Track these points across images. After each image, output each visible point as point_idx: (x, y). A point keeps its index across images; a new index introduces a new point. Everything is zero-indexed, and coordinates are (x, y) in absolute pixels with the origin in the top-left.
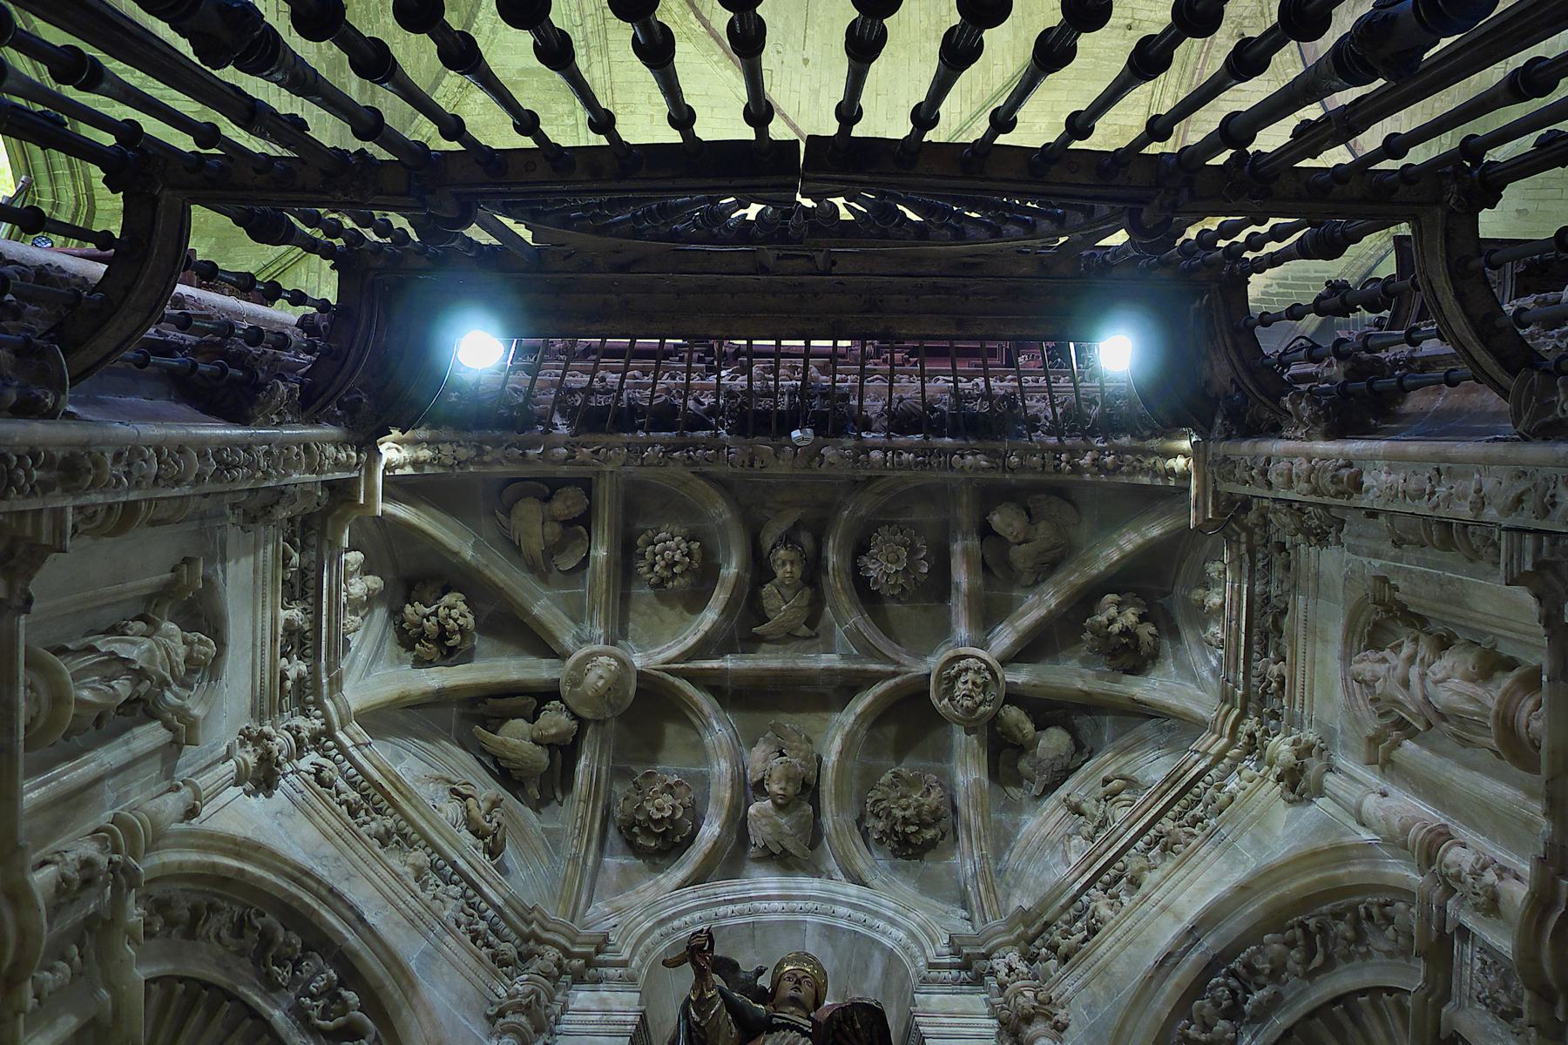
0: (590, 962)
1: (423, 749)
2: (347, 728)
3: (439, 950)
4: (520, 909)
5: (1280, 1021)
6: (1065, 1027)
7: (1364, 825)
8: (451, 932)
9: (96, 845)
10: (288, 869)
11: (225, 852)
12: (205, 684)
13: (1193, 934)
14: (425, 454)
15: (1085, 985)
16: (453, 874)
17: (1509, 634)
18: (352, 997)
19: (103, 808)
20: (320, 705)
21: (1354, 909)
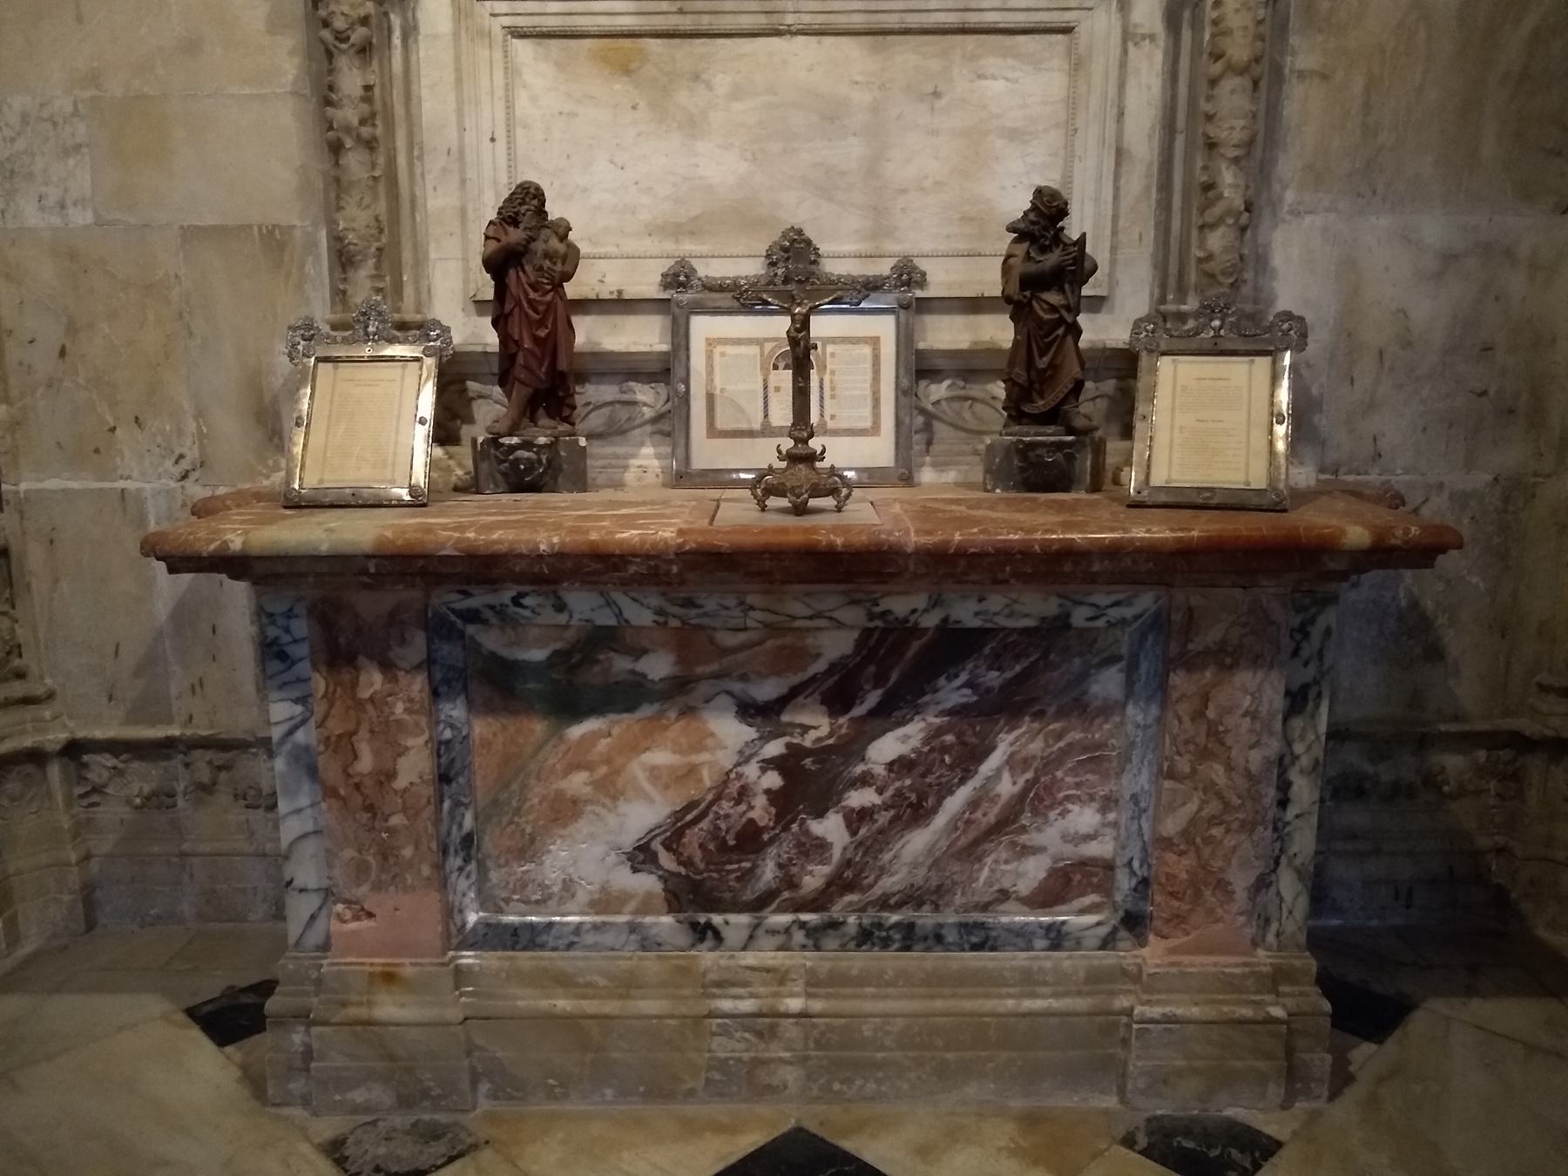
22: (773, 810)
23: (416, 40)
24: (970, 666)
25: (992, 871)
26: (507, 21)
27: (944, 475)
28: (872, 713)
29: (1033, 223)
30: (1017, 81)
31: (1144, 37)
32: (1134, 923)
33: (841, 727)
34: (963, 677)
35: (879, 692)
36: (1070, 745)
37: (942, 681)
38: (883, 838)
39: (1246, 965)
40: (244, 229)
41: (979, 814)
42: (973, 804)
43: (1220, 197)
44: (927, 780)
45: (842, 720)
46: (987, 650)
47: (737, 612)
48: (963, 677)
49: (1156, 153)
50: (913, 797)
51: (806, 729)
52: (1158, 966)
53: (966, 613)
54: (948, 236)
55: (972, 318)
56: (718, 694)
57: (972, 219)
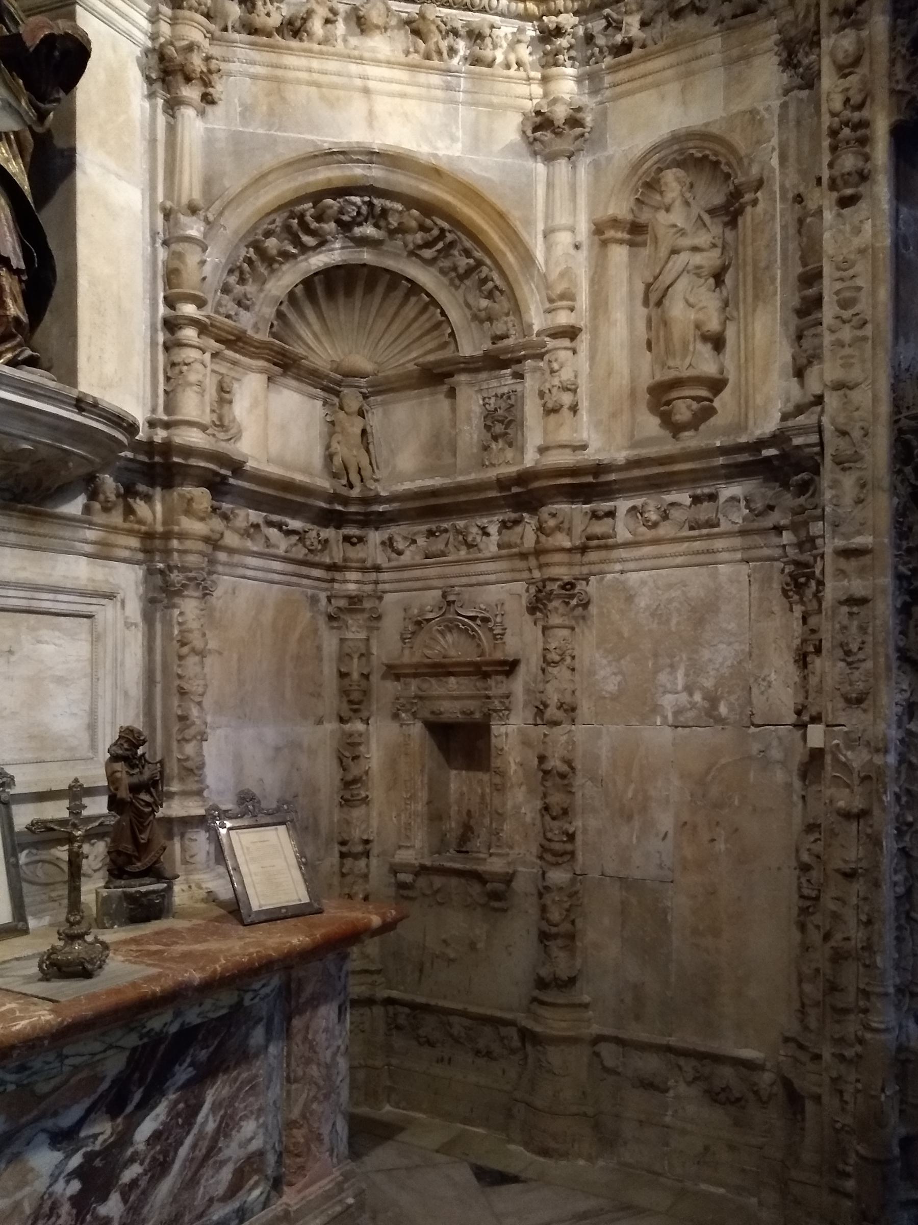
5: (367, 256)
6: (213, 102)
7: (545, 237)
13: (372, 156)
15: (254, 77)
17: (742, 347)
21: (479, 263)
22: (74, 1211)
24: (191, 1051)
25: (205, 1187)
27: (43, 920)
28: (138, 1107)
29: (127, 750)
30: (61, 646)
31: (132, 624)
32: (277, 1184)
33: (118, 1126)
34: (188, 1060)
35: (141, 1090)
36: (242, 1083)
37: (177, 1067)
38: (145, 1194)
39: (332, 1180)
41: (197, 1152)
42: (194, 1147)
43: (193, 723)
44: (169, 1141)
45: (120, 1120)
46: (200, 1037)
47: (57, 1064)
48: (188, 1060)
49: (141, 694)
50: (161, 1158)
51: (95, 1136)
52: (296, 1204)
53: (192, 1017)
54: (21, 749)
55: (39, 805)
56: (35, 1135)
57: (35, 737)
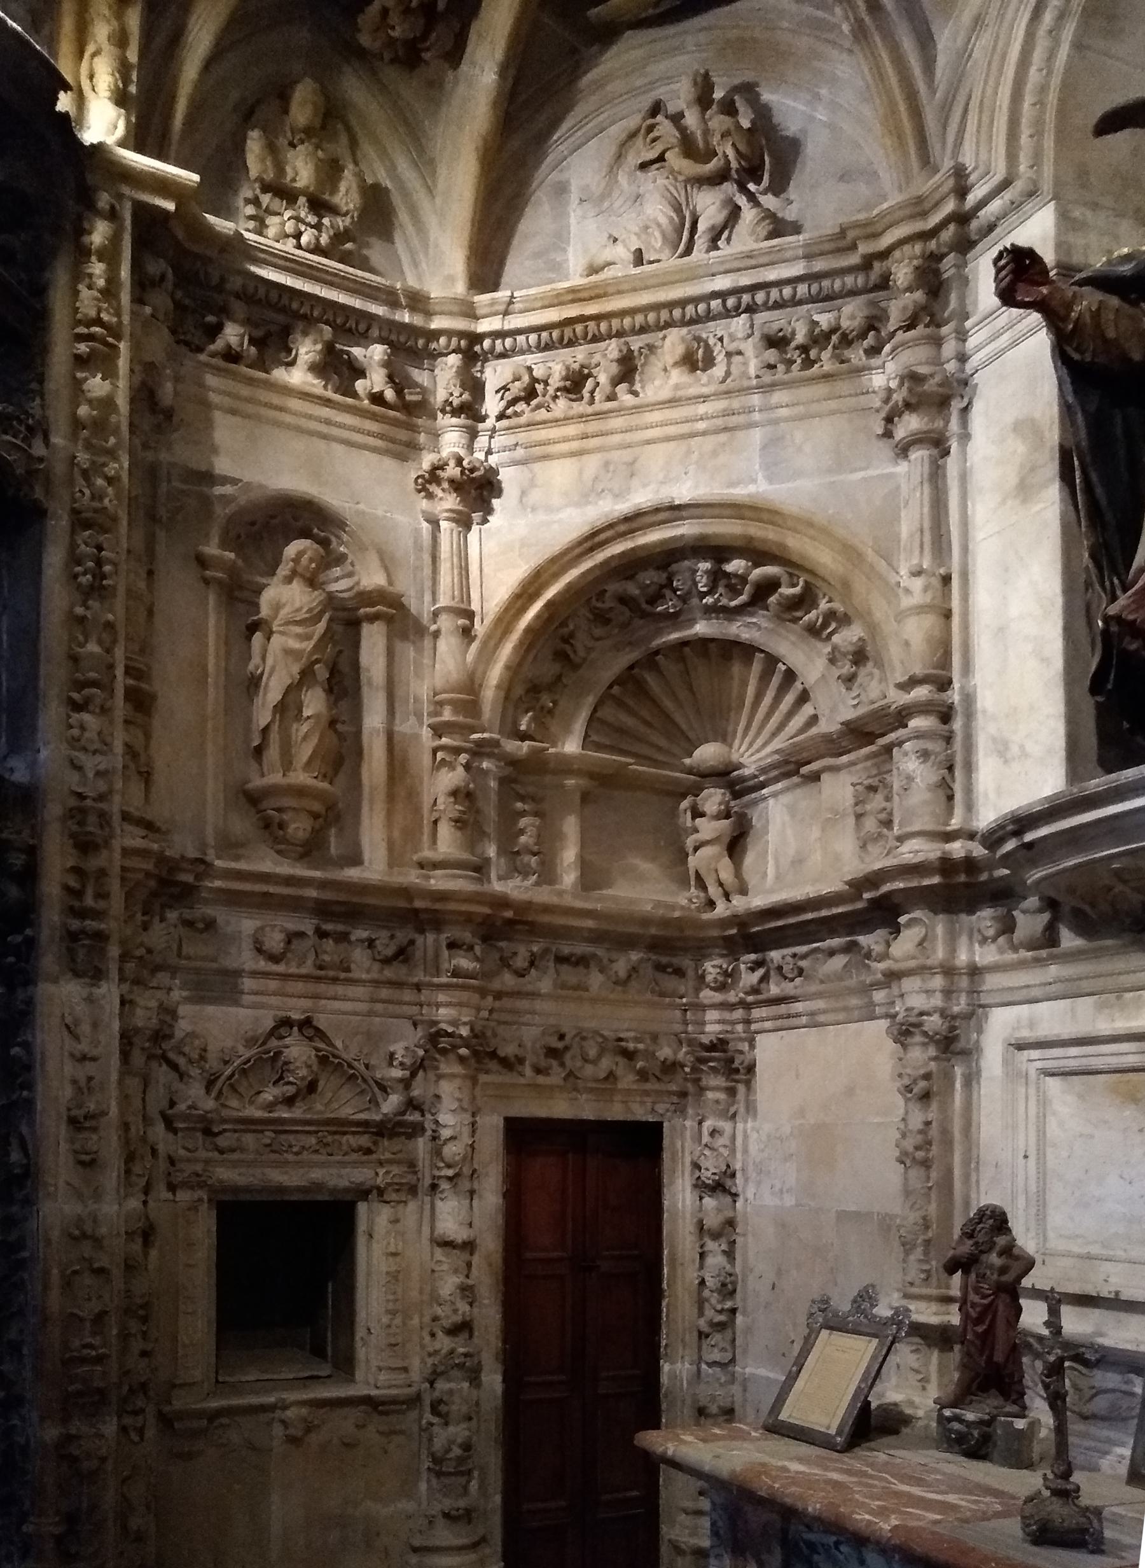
0: (962, 218)
1: (579, 125)
2: (479, 312)
3: (775, 422)
4: (827, 247)
8: (773, 386)
9: (444, 770)
10: (577, 551)
11: (523, 610)
12: (345, 537)
14: (101, 32)
16: (724, 302)
18: (736, 566)
19: (417, 737)
20: (435, 335)
23: (979, 1083)
26: (1039, 1065)
40: (869, 1214)
